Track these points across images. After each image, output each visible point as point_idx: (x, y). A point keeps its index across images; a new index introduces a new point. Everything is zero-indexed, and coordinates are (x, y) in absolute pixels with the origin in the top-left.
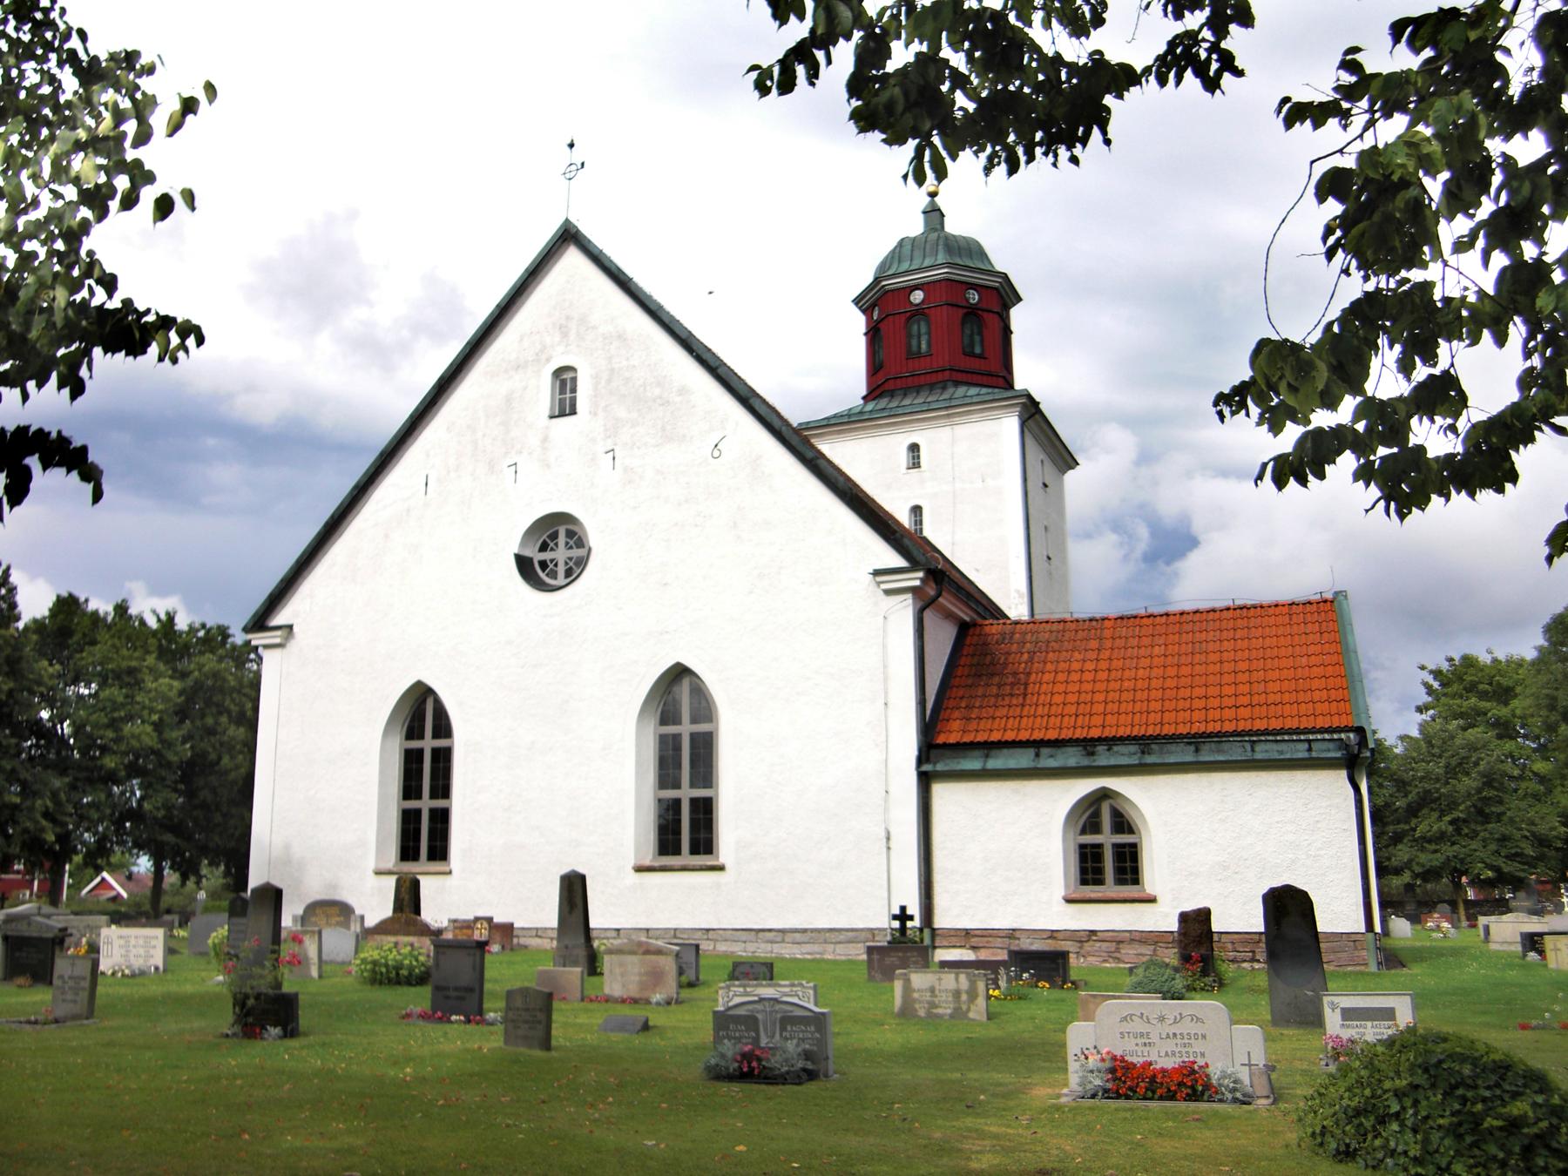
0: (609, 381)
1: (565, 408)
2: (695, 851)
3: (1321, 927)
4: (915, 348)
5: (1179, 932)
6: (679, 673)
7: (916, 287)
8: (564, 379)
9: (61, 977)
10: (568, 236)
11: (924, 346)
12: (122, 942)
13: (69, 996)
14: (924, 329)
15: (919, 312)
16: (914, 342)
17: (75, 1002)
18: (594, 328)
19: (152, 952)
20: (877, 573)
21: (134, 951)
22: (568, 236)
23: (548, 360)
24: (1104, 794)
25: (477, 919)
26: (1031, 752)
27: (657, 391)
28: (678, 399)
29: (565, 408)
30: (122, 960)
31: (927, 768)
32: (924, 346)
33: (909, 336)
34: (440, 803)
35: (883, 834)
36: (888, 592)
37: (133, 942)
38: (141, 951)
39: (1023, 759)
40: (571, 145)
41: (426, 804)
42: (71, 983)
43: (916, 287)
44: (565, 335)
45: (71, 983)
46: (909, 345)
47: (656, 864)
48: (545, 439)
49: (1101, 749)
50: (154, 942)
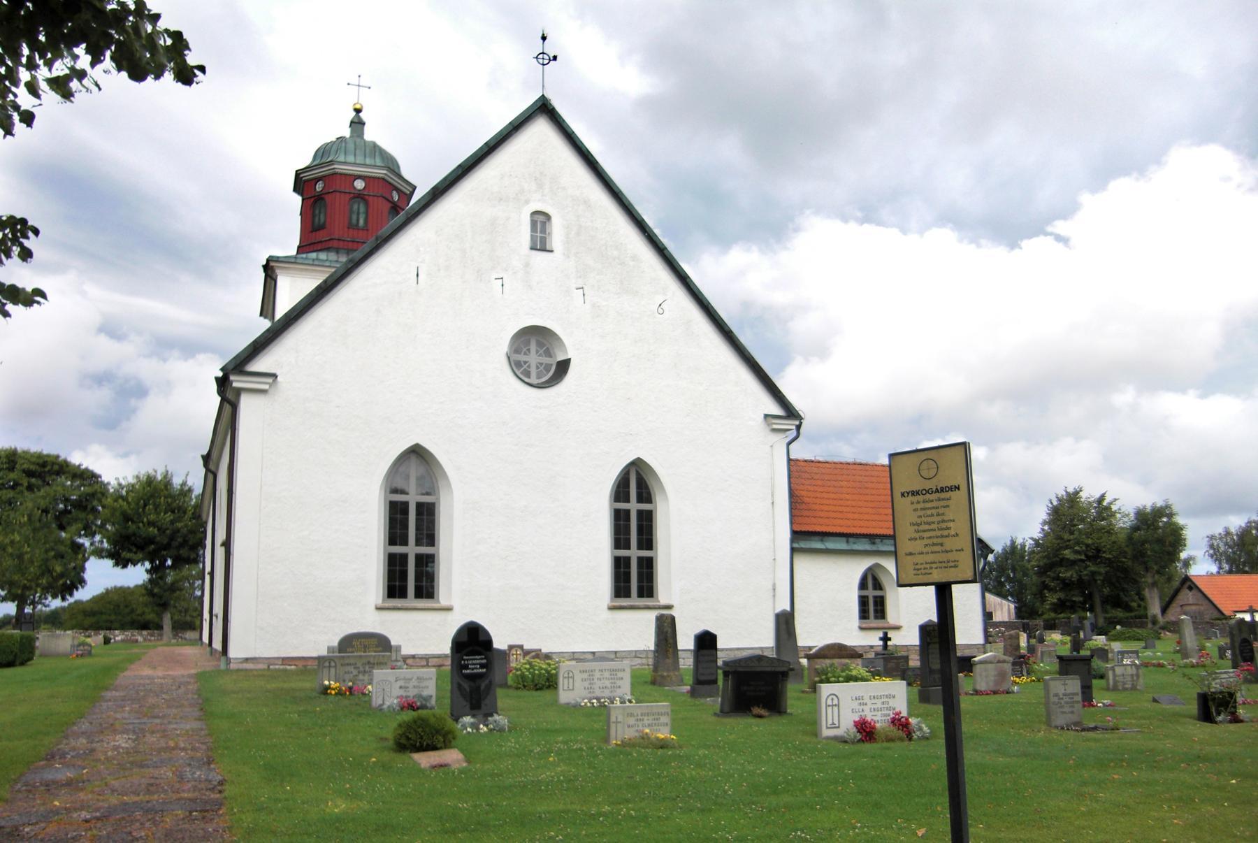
0: (578, 234)
1: (540, 244)
2: (641, 595)
3: (799, 644)
4: (354, 221)
5: (656, 651)
6: (417, 453)
7: (359, 177)
8: (540, 221)
9: (1056, 695)
10: (543, 108)
11: (361, 222)
12: (585, 676)
13: (1067, 709)
14: (362, 209)
15: (360, 196)
16: (354, 217)
17: (1072, 712)
18: (564, 188)
19: (619, 683)
20: (766, 416)
21: (599, 684)
22: (543, 108)
23: (527, 202)
24: (877, 565)
25: (511, 647)
26: (844, 539)
27: (616, 253)
28: (631, 263)
29: (540, 244)
30: (585, 693)
31: (796, 545)
32: (361, 222)
33: (351, 212)
34: (622, 553)
35: (771, 587)
36: (774, 430)
37: (597, 674)
38: (608, 683)
39: (840, 544)
40: (544, 38)
41: (411, 550)
42: (1066, 699)
43: (359, 177)
44: (540, 186)
45: (1066, 699)
46: (350, 219)
47: (386, 605)
48: (527, 265)
49: (878, 541)
50: (620, 674)
